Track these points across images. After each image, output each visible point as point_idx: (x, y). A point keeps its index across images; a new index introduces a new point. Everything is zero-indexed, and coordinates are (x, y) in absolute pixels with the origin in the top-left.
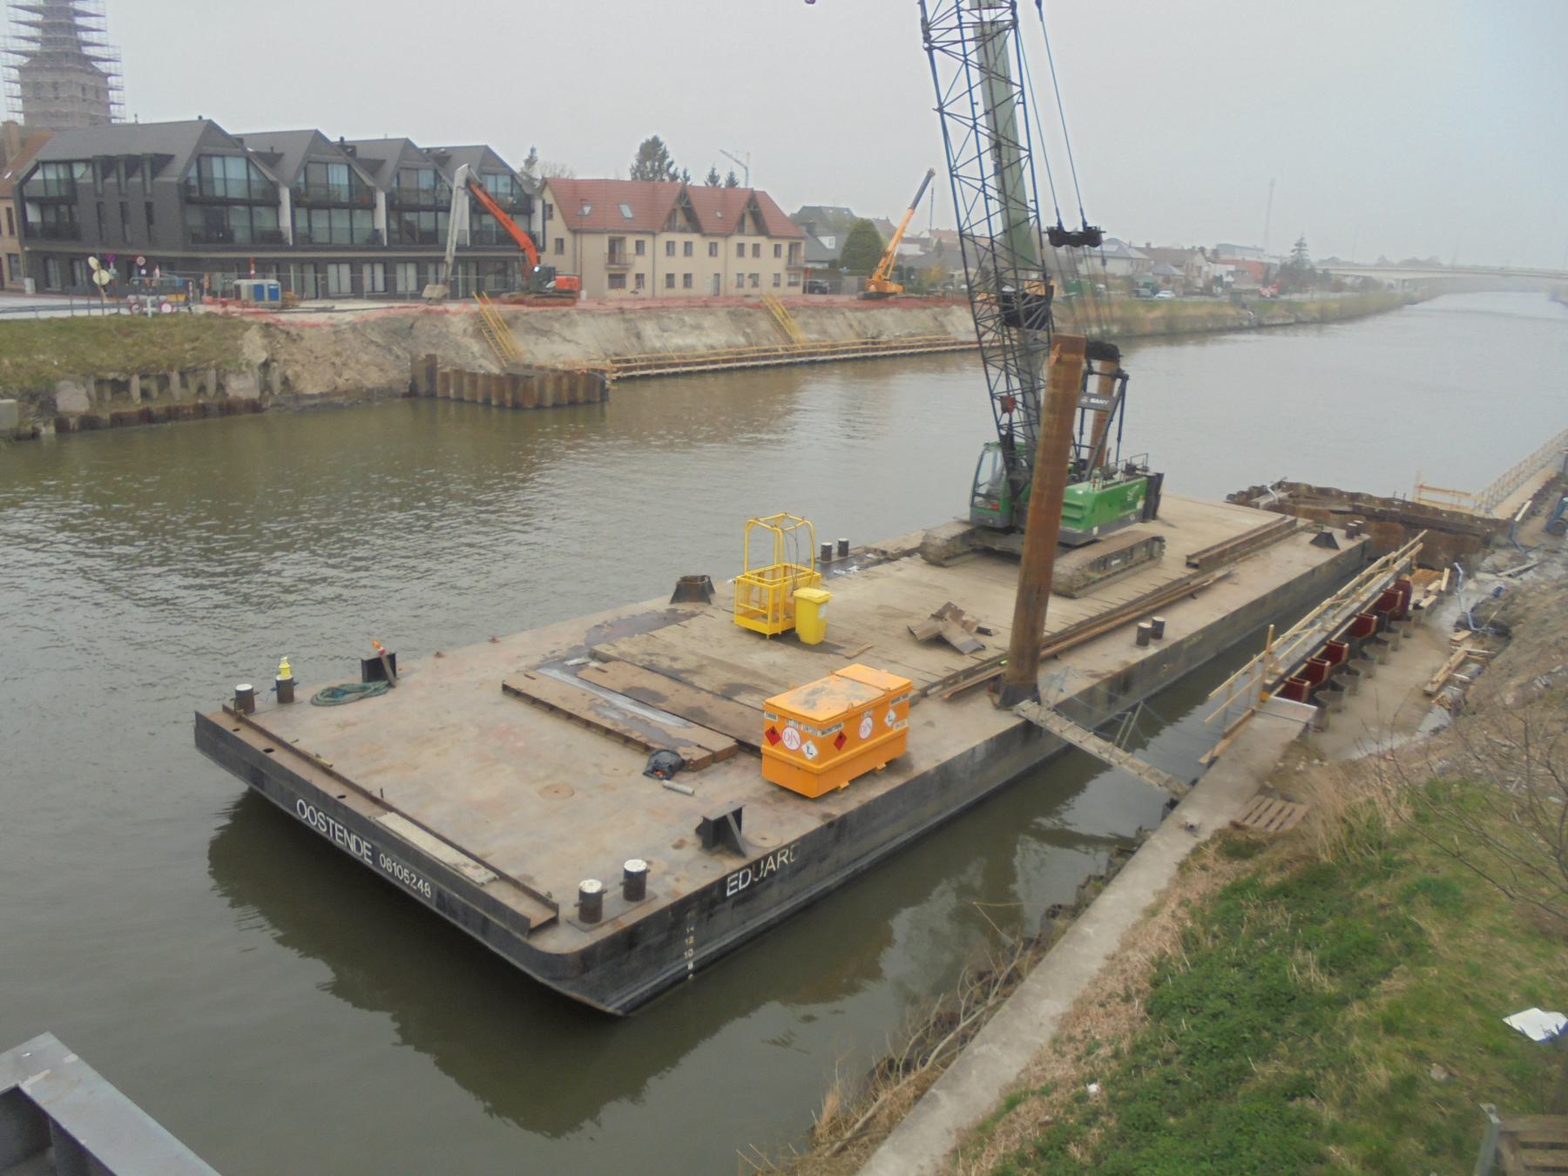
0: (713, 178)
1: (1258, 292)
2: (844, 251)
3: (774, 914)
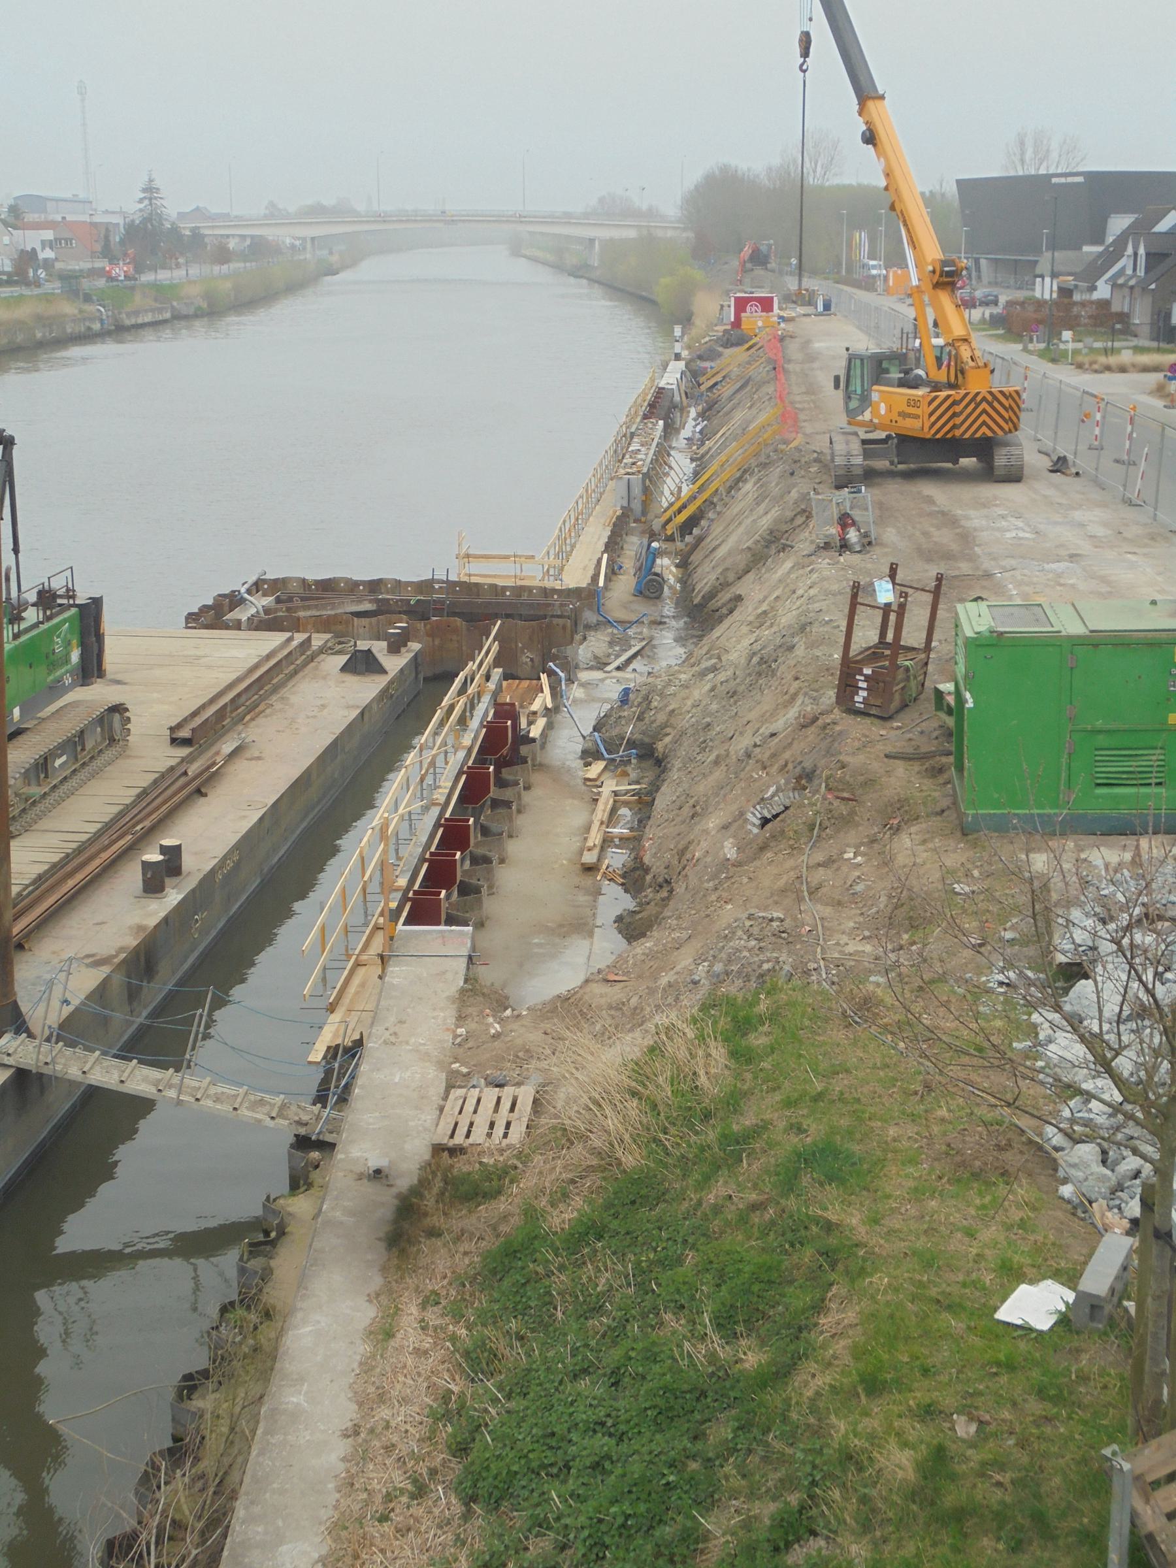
1: (101, 273)
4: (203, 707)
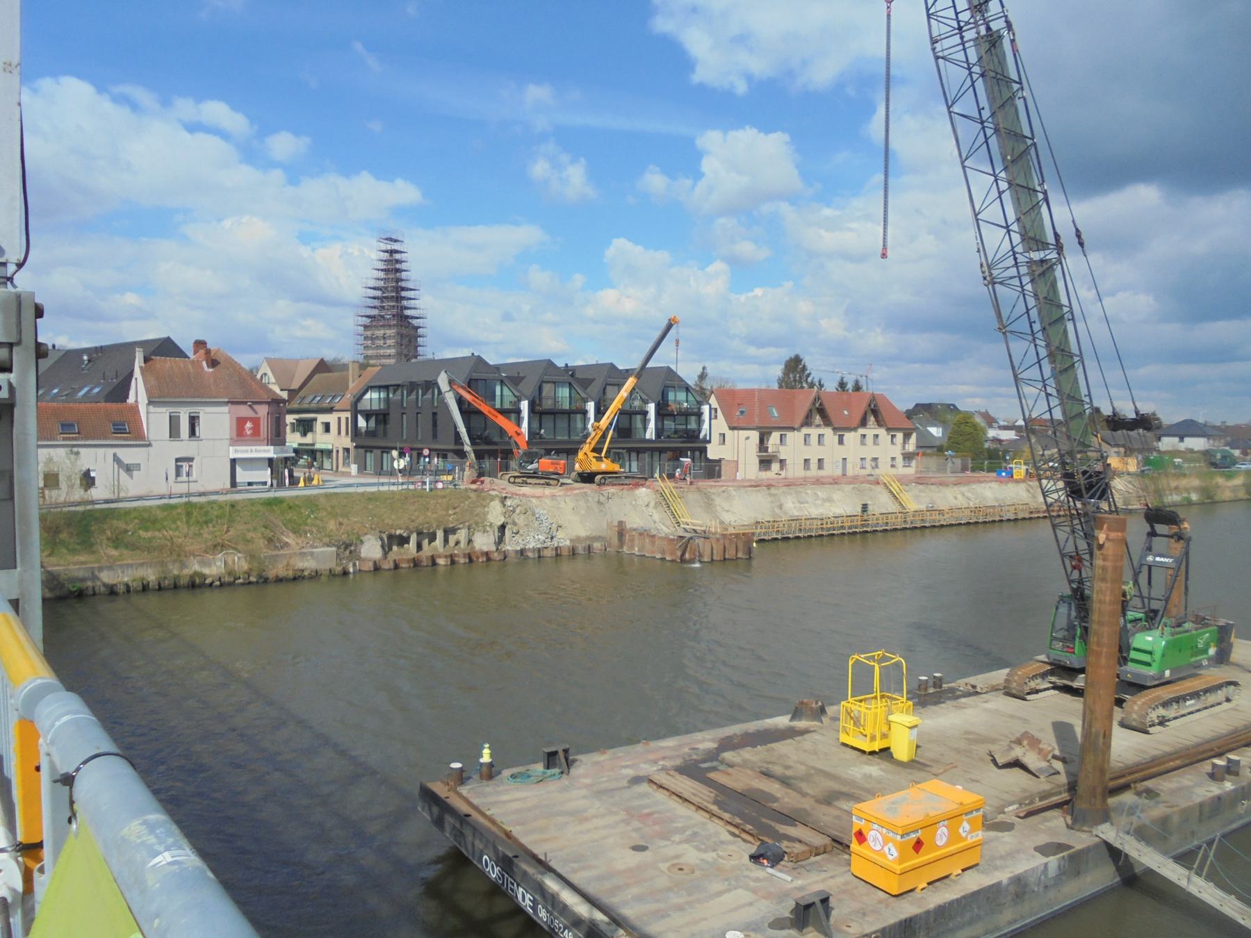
0: (842, 385)
2: (950, 438)
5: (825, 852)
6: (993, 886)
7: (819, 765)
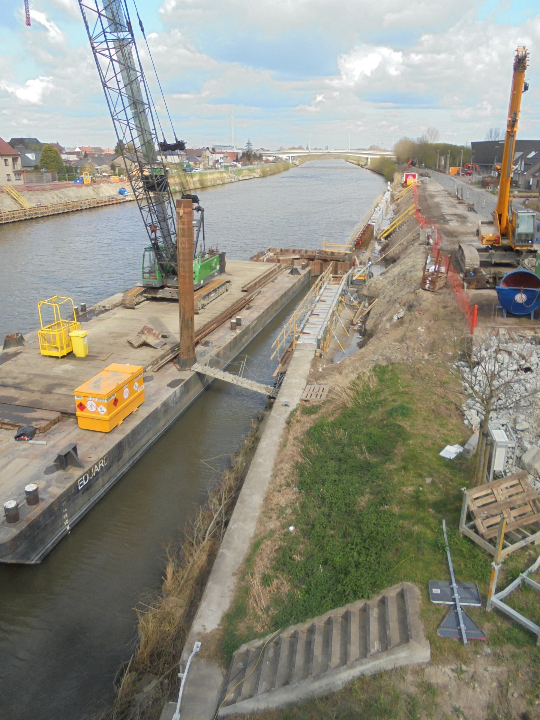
3: (102, 491)
4: (251, 282)
5: (59, 421)
6: (154, 410)
7: (35, 372)
